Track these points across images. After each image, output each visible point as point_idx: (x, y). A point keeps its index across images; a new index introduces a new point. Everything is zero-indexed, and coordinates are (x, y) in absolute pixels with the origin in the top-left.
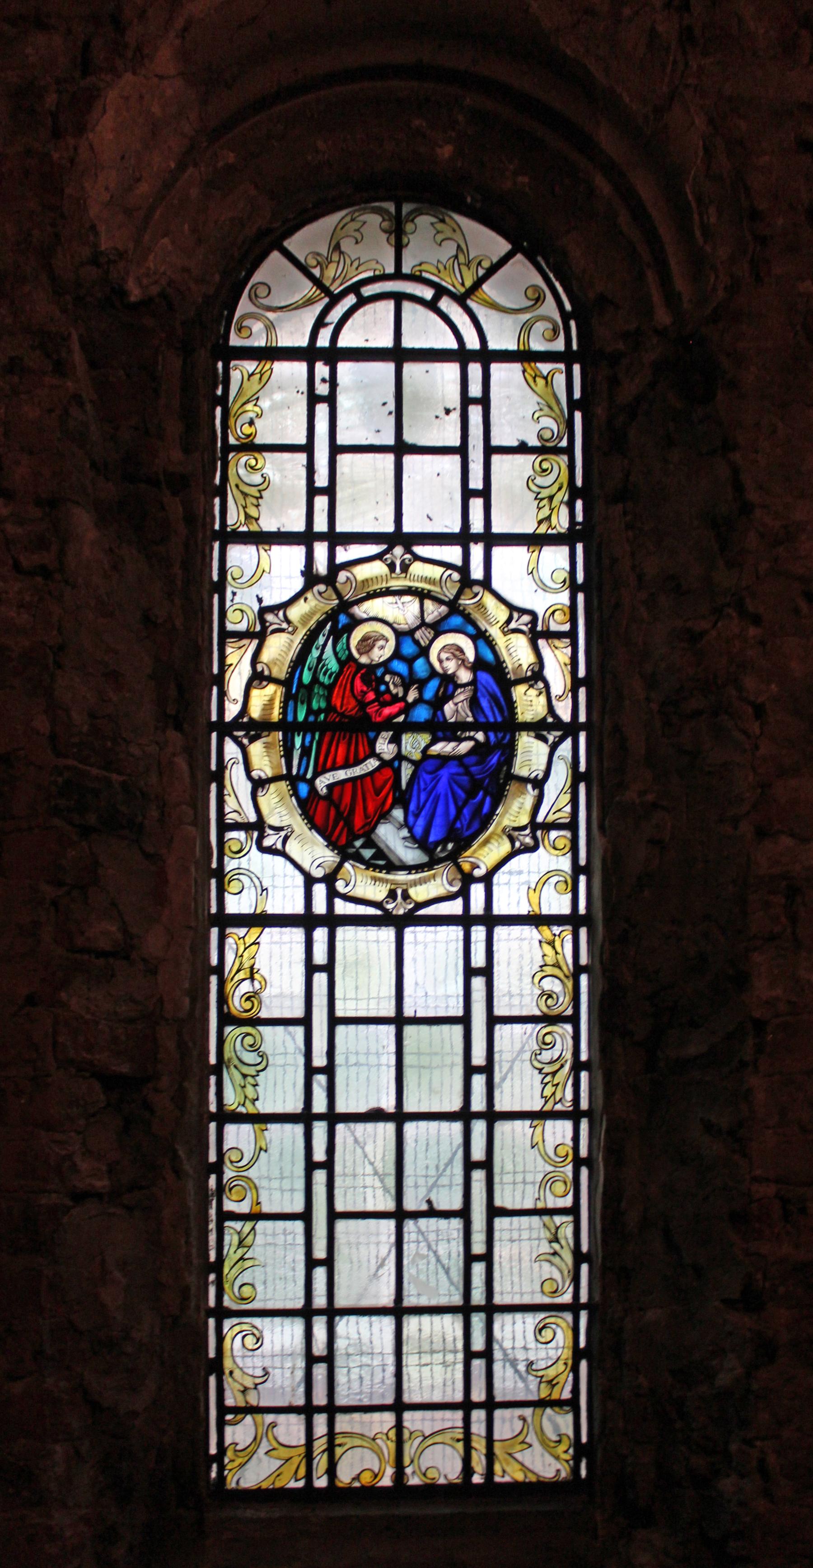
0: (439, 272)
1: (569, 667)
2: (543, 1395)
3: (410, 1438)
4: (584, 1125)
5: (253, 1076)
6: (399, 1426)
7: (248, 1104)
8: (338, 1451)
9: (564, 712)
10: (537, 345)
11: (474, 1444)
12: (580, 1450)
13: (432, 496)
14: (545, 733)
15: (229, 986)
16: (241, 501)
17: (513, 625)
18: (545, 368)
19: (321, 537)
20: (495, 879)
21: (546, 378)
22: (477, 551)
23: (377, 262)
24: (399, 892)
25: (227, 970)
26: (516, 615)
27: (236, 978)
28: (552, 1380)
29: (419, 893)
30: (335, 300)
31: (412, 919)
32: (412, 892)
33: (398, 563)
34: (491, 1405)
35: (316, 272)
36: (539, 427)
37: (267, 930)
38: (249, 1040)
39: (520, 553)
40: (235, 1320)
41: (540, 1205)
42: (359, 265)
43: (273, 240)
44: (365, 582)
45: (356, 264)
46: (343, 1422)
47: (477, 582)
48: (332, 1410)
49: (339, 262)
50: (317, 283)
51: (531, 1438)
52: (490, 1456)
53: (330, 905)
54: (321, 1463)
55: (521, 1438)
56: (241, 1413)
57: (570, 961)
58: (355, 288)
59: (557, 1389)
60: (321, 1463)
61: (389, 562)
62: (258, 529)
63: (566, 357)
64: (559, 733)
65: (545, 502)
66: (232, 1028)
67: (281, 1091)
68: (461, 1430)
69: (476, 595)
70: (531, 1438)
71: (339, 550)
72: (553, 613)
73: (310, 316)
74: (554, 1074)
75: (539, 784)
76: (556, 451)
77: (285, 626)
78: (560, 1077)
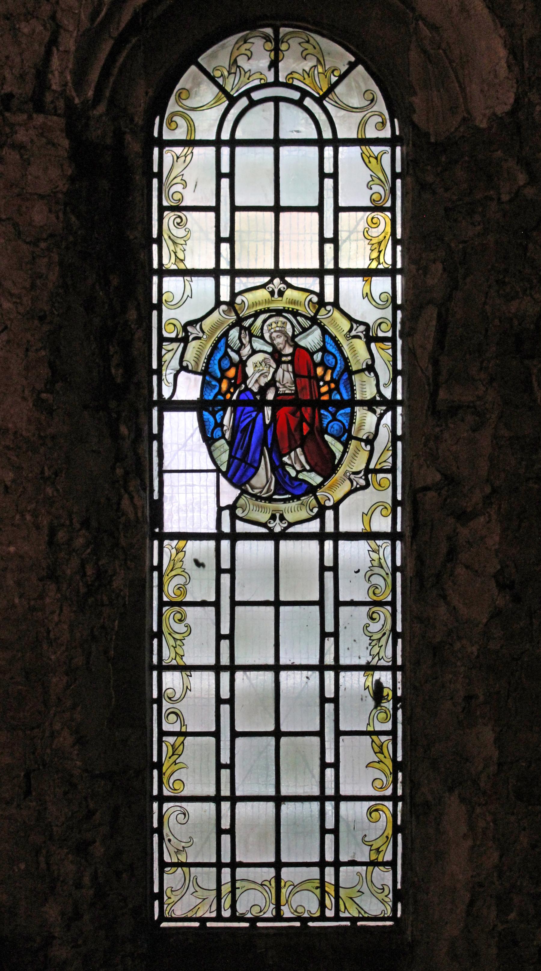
0: (304, 79)
1: (391, 363)
2: (373, 857)
3: (285, 886)
4: (399, 675)
5: (181, 640)
6: (278, 878)
7: (178, 658)
8: (238, 892)
9: (387, 393)
10: (371, 133)
11: (327, 889)
12: (397, 896)
13: (300, 247)
14: (375, 407)
15: (165, 579)
16: (172, 248)
17: (353, 333)
18: (376, 150)
19: (225, 272)
20: (341, 507)
21: (376, 158)
22: (329, 280)
23: (261, 74)
24: (278, 515)
25: (164, 569)
26: (355, 326)
27: (170, 575)
28: (379, 848)
29: (263, 294)
30: (233, 101)
31: (285, 535)
32: (286, 516)
33: (276, 291)
34: (337, 864)
35: (220, 81)
36: (371, 192)
37: (366, 267)
38: (178, 616)
39: (358, 282)
40: (171, 804)
41: (370, 729)
42: (250, 76)
43: (191, 58)
44: (255, 304)
45: (248, 75)
46: (240, 872)
47: (329, 304)
48: (234, 865)
49: (235, 73)
50: (222, 89)
51: (365, 889)
52: (337, 897)
53: (233, 526)
54: (227, 902)
55: (358, 888)
56: (175, 866)
57: (390, 564)
58: (247, 93)
59: (382, 854)
60: (227, 902)
61: (270, 289)
62: (184, 268)
63: (391, 142)
64: (384, 408)
65: (376, 246)
66: (167, 608)
67: (199, 649)
68: (318, 881)
69: (329, 311)
70: (365, 889)
71: (237, 280)
72: (380, 325)
73: (216, 113)
74: (379, 640)
75: (370, 441)
76: (381, 209)
77: (352, 477)
78: (383, 641)
